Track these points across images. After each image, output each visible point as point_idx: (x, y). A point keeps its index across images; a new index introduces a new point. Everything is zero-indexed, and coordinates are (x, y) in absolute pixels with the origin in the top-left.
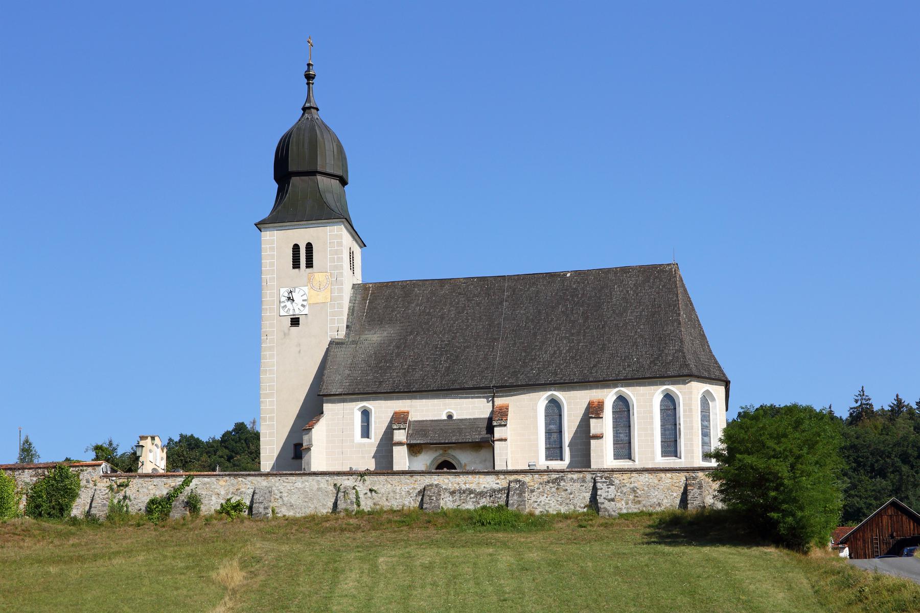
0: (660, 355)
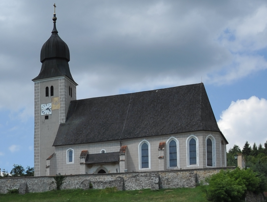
0: (190, 122)
